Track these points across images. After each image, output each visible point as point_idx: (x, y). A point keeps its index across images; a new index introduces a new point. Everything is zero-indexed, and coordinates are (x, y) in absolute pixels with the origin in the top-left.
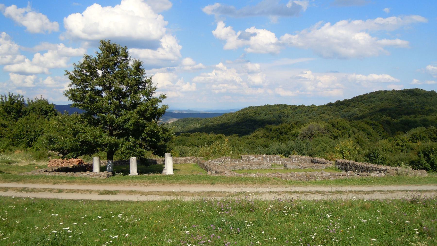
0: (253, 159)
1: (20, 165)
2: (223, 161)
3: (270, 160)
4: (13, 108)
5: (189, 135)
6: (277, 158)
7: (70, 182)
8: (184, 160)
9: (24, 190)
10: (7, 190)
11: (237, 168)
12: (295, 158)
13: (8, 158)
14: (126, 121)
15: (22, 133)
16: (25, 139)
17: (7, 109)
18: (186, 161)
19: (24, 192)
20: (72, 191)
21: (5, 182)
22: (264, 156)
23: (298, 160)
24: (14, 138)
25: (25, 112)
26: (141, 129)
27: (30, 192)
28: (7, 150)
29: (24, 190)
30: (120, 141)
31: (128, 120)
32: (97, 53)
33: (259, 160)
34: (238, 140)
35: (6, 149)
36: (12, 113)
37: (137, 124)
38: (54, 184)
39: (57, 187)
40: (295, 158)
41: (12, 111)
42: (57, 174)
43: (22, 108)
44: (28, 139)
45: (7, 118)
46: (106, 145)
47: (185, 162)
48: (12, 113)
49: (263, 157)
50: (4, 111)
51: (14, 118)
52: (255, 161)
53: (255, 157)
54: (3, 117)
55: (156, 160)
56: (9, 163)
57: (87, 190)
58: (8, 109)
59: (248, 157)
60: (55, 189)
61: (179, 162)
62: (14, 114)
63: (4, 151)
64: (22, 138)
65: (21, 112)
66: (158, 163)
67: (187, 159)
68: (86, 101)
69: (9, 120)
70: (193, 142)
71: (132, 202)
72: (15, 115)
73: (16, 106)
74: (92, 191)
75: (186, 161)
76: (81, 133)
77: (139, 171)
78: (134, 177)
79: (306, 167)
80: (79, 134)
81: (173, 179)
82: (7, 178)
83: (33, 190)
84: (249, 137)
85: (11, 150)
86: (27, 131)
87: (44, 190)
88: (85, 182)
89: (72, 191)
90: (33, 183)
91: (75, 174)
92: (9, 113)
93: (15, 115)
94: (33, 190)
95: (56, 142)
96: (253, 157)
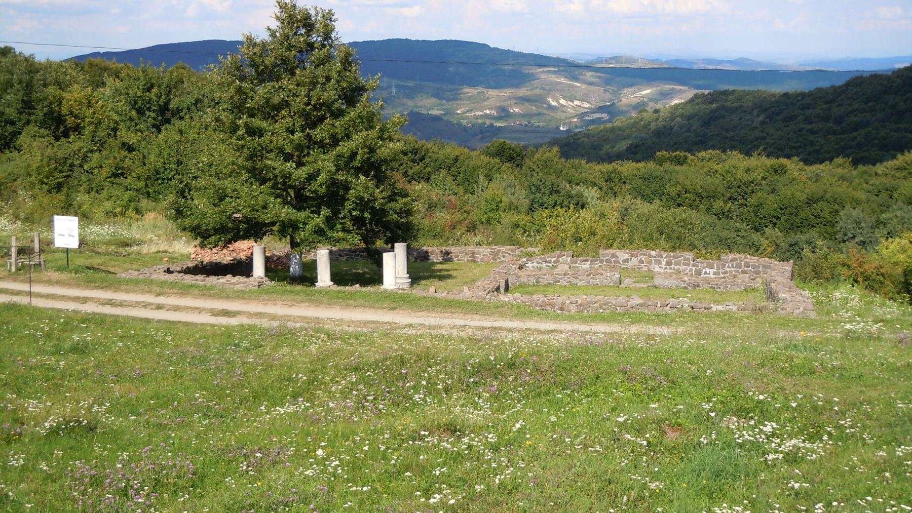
0: (626, 261)
1: (145, 249)
2: (555, 262)
3: (669, 263)
4: (150, 100)
5: (686, 158)
6: (686, 259)
7: (182, 293)
8: (492, 253)
9: (110, 303)
10: (86, 302)
11: (543, 282)
12: (732, 261)
13: (124, 232)
14: (312, 177)
15: (167, 166)
16: (173, 182)
17: (136, 102)
18: (495, 255)
19: (109, 306)
20: (176, 308)
21: (87, 288)
22: (653, 253)
23: (739, 266)
24: (149, 178)
25: (179, 110)
26: (341, 192)
27: (117, 306)
28: (131, 212)
29: (110, 303)
30: (302, 215)
31: (318, 173)
32: (269, 29)
33: (641, 262)
34: (842, 178)
35: (126, 207)
36: (147, 113)
37: (333, 183)
38: (158, 295)
39: (161, 300)
40: (732, 261)
41: (149, 109)
42: (189, 279)
43: (170, 100)
44: (181, 183)
45: (136, 125)
46: (273, 224)
47: (494, 259)
48: (147, 113)
49: (651, 256)
50: (127, 108)
51: (154, 126)
52: (630, 264)
53: (632, 255)
54: (128, 123)
55: (427, 252)
56: (127, 245)
57: (196, 308)
58: (140, 103)
59: (614, 256)
60: (152, 304)
61: (480, 257)
62: (153, 115)
63: (123, 214)
64: (168, 179)
65: (168, 110)
66: (431, 257)
67: (499, 251)
68: (240, 133)
69: (142, 132)
70: (688, 183)
71: (196, 325)
72: (154, 119)
73: (156, 95)
74: (204, 309)
75: (495, 255)
76: (231, 197)
77: (338, 278)
78: (325, 292)
79: (698, 286)
80: (227, 199)
81: (396, 301)
82: (91, 282)
83: (121, 304)
84: (880, 172)
85: (138, 211)
86: (179, 163)
87: (138, 304)
88: (203, 295)
89: (176, 308)
90: (126, 291)
91: (207, 279)
92: (140, 112)
93: (154, 119)
94: (121, 304)
95: (189, 213)
96: (626, 256)
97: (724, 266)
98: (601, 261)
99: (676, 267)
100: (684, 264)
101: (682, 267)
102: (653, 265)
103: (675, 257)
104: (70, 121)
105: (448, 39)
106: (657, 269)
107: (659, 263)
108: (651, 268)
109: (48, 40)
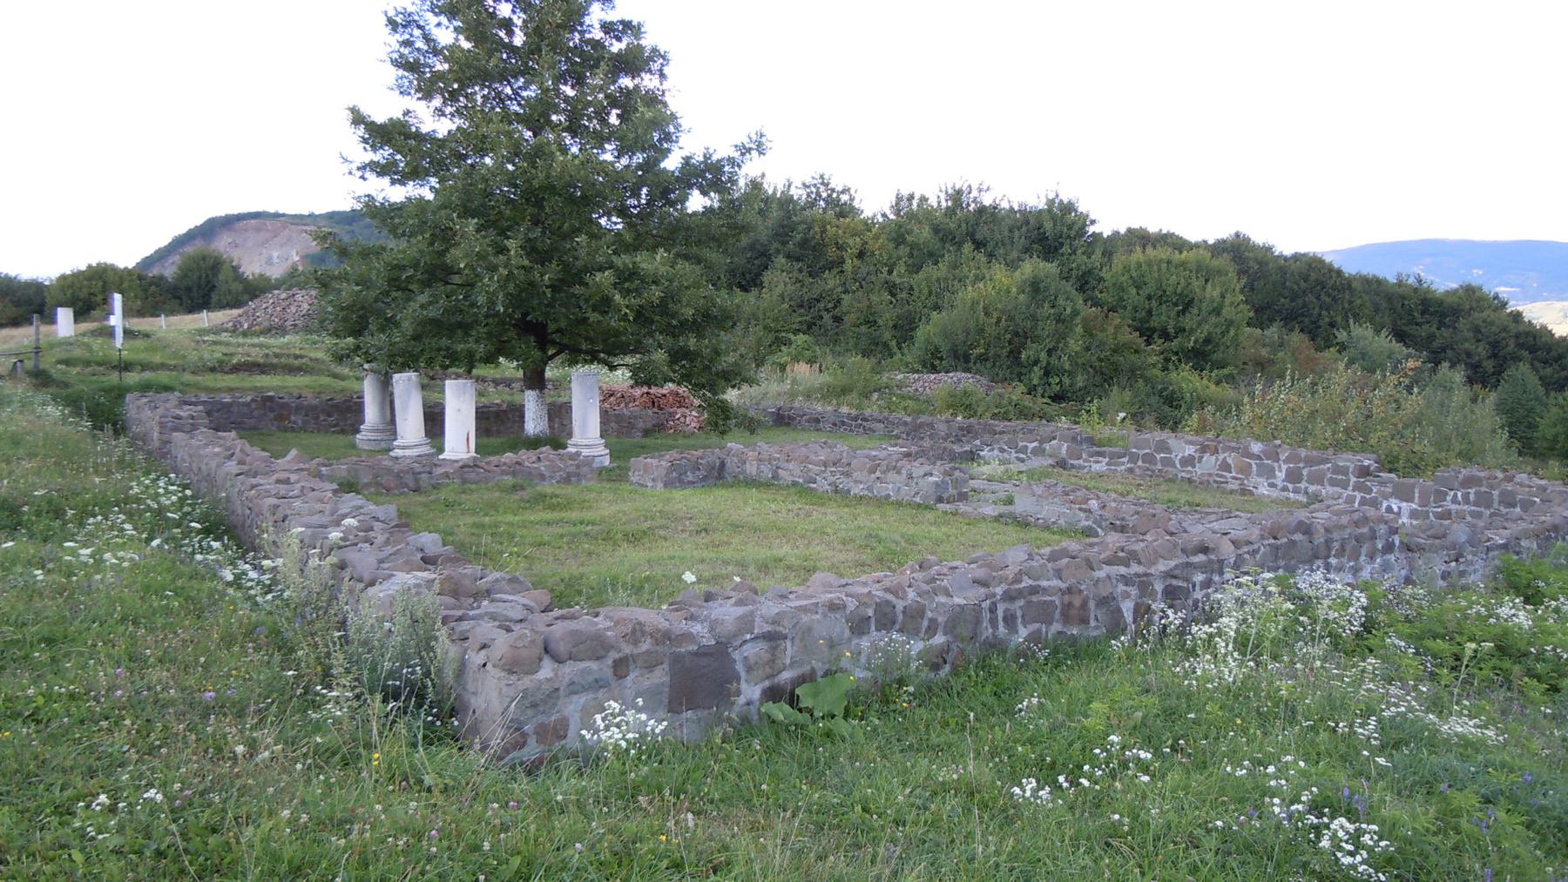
0: (1188, 461)
3: (1294, 477)
32: (358, 119)
33: (1225, 467)
52: (1199, 470)
53: (1203, 449)
96: (1190, 450)
97: (1441, 496)
98: (1134, 458)
99: (1312, 488)
100: (1333, 483)
101: (1327, 490)
102: (1254, 479)
103: (1310, 462)
104: (832, 252)
105: (199, 222)
106: (1264, 490)
107: (1269, 473)
108: (1250, 483)
109: (42, 263)
